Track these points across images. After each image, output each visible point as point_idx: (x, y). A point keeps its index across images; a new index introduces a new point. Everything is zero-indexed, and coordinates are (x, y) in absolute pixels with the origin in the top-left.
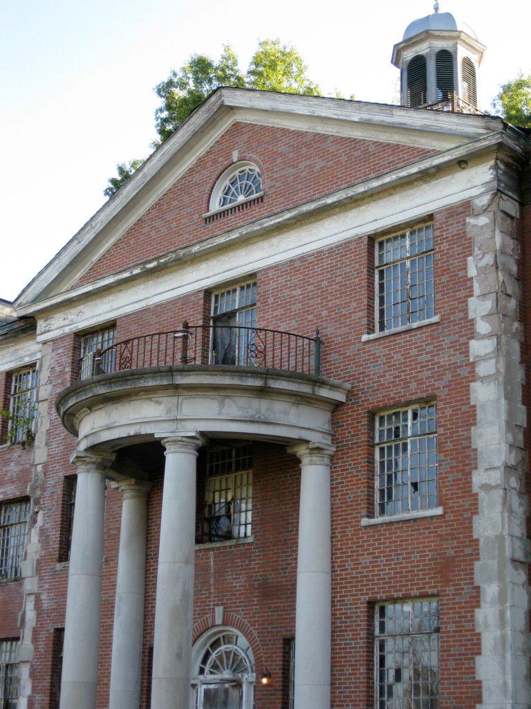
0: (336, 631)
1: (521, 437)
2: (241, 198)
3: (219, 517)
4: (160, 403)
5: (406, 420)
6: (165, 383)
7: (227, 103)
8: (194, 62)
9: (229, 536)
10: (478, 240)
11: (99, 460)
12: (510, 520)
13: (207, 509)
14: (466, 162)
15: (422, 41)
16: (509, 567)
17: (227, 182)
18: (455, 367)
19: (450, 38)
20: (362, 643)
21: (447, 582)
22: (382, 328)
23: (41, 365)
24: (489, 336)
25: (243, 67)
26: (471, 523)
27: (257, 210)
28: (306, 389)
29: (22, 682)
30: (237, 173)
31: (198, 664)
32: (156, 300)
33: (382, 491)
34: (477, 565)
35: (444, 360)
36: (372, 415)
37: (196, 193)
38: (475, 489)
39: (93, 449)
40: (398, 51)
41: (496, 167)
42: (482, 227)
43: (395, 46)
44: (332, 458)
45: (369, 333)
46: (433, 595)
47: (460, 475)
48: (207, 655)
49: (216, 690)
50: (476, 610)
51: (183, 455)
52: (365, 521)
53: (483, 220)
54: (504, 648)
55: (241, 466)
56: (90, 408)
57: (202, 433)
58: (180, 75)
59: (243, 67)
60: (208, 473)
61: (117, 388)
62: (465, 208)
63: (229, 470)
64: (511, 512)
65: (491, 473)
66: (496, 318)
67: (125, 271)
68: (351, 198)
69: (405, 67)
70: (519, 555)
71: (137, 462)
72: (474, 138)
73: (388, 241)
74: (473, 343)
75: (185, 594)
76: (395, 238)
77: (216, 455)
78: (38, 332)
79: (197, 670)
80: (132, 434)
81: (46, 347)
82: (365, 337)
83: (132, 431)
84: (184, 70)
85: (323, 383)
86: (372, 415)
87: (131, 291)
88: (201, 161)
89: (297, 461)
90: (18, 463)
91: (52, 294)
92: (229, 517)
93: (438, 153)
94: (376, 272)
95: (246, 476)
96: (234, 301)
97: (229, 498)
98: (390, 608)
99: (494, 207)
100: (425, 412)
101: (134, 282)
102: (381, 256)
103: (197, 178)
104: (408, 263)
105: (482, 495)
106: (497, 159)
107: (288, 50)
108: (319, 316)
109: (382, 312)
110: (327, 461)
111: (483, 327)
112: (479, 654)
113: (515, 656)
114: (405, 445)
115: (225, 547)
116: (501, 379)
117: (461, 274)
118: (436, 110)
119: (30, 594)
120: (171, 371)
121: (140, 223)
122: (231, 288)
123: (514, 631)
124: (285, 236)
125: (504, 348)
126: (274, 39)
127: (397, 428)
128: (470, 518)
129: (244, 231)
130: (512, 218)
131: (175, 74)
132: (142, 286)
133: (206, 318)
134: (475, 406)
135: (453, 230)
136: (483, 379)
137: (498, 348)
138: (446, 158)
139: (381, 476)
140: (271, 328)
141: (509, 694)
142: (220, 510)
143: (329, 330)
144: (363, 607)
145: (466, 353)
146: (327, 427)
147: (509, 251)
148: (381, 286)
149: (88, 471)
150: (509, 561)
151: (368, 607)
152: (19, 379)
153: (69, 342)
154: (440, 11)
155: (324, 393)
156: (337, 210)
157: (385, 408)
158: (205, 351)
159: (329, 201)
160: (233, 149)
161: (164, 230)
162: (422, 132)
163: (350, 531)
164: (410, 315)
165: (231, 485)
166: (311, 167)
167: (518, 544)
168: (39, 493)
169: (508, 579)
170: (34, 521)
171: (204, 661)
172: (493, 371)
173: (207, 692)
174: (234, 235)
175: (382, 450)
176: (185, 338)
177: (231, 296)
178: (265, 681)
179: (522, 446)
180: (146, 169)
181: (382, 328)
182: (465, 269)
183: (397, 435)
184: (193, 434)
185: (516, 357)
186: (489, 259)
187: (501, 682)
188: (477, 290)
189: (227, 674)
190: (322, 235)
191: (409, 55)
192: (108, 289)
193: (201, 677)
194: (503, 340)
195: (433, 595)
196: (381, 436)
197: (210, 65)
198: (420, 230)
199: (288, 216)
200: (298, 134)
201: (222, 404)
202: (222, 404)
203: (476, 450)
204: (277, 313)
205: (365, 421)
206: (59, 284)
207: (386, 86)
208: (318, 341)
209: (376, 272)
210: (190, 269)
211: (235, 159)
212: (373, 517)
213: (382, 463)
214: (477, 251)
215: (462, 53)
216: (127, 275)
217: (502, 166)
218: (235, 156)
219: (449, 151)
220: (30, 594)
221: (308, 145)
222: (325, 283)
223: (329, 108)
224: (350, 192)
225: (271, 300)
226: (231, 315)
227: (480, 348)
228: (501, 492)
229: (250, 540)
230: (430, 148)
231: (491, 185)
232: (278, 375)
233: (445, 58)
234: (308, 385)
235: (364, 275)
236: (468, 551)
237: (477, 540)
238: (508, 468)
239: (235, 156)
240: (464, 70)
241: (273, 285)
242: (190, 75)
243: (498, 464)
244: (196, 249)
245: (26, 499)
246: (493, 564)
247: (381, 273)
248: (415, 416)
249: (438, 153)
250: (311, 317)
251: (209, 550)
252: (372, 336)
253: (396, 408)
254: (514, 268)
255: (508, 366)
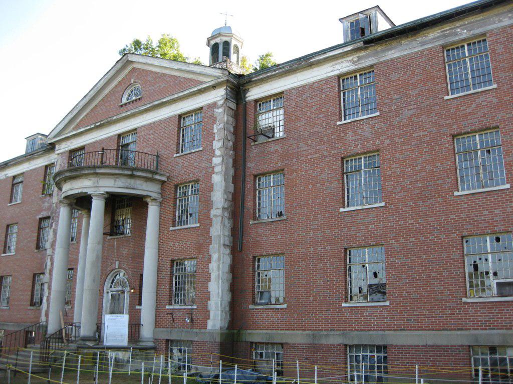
0: (159, 272)
1: (230, 196)
2: (134, 98)
3: (120, 226)
4: (91, 180)
5: (189, 188)
6: (92, 172)
7: (130, 60)
8: (134, 41)
9: (123, 233)
10: (218, 118)
11: (69, 202)
12: (223, 229)
13: (115, 223)
14: (215, 87)
15: (218, 37)
16: (222, 247)
17: (129, 92)
18: (207, 168)
19: (229, 36)
20: (168, 276)
21: (199, 253)
22: (182, 152)
23: (57, 163)
24: (220, 156)
25: (155, 44)
26: (209, 230)
27: (139, 103)
28: (150, 175)
29: (45, 291)
30: (133, 88)
31: (110, 284)
32: (100, 138)
33: (179, 217)
34: (211, 246)
35: (203, 165)
36: (176, 186)
37: (117, 96)
38: (212, 216)
39: (66, 197)
40: (209, 40)
41: (226, 89)
42: (220, 113)
43: (208, 39)
44: (161, 203)
45: (177, 154)
46: (194, 258)
47: (206, 211)
48: (113, 280)
49: (115, 294)
50: (210, 264)
51: (99, 201)
52: (171, 228)
53: (220, 110)
54: (219, 278)
55: (129, 205)
56: (65, 181)
57: (107, 192)
58: (129, 46)
59: (155, 44)
60: (116, 207)
61: (74, 174)
62: (214, 105)
63: (124, 207)
64: (224, 226)
65: (218, 210)
66: (222, 149)
67: (88, 126)
68: (173, 99)
69: (211, 47)
70: (227, 243)
71: (82, 202)
72: (218, 78)
73: (187, 117)
74: (214, 159)
75: (97, 256)
76: (189, 116)
77: (114, 202)
78: (56, 150)
79: (109, 286)
80: (80, 192)
81: (59, 156)
82: (175, 155)
83: (79, 191)
84: (131, 44)
85: (157, 173)
86: (176, 186)
87: (91, 134)
88: (120, 83)
89: (146, 204)
90: (48, 203)
91: (64, 133)
92: (123, 225)
93: (206, 83)
94: (182, 129)
95: (129, 209)
96: (129, 139)
97: (124, 218)
98: (262, 259)
99: (225, 105)
100: (196, 186)
101: (92, 131)
102: (184, 123)
103: (118, 89)
104: (193, 126)
105: (214, 219)
106: (227, 86)
107: (173, 38)
108: (159, 146)
109: (182, 145)
110: (158, 204)
111: (218, 153)
112: (210, 281)
113: (223, 282)
114: (188, 198)
115: (121, 238)
116: (223, 173)
117: (211, 131)
118: (215, 67)
119: (49, 255)
120: (94, 167)
121: (97, 108)
122: (128, 134)
123: (223, 272)
124: (148, 114)
125: (225, 162)
126: (168, 34)
127: (186, 192)
128: (209, 228)
129: (133, 111)
130: (233, 109)
131: (127, 46)
132: (95, 132)
133: (118, 146)
134: (213, 184)
135: (209, 114)
136: (217, 173)
137: (223, 161)
138: (208, 85)
139: (179, 210)
140: (141, 151)
141: (220, 297)
142: (118, 221)
143: (163, 152)
144: (169, 262)
145: (211, 163)
146: (159, 191)
147: (231, 123)
148: (183, 135)
149: (64, 207)
150: (222, 245)
151: (345, 251)
152: (50, 169)
153: (67, 154)
154: (227, 25)
155: (158, 177)
156: (168, 104)
157: (181, 184)
158: (117, 159)
159: (164, 100)
160: (131, 78)
161: (104, 110)
162: (200, 74)
163: (166, 232)
164: (192, 147)
165: (125, 213)
166: (160, 86)
167: (227, 238)
168: (54, 214)
169: (222, 252)
170: (52, 226)
171: (112, 283)
172: (220, 170)
173: (112, 294)
174: (129, 113)
175: (180, 200)
176: (102, 154)
177: (128, 138)
178: (132, 291)
179: (231, 200)
180: (98, 85)
181: (182, 152)
182: (213, 129)
183: (185, 195)
184: (103, 193)
185: (231, 165)
186: (222, 126)
187: (217, 292)
188: (216, 138)
189: (120, 288)
190: (162, 114)
191: (212, 42)
192: (81, 133)
193: (111, 289)
194: (225, 158)
195: (194, 258)
196: (180, 195)
197: (140, 43)
198: (198, 113)
199: (149, 106)
200: (156, 73)
201: (115, 181)
202: (115, 181)
203: (213, 201)
204: (144, 145)
205: (173, 189)
206: (65, 130)
207: (205, 56)
208: (158, 156)
209: (182, 129)
210: (113, 126)
211: (132, 82)
212: (175, 227)
213: (179, 205)
214: (218, 122)
215: (233, 43)
216: (89, 128)
217: (229, 89)
218: (132, 81)
219: (209, 82)
220: (49, 255)
221: (160, 78)
222: (162, 133)
223: (166, 63)
224: (172, 97)
225: (142, 140)
226: (128, 145)
227: (216, 161)
228: (221, 218)
229: (130, 235)
230: (203, 81)
231: (224, 96)
232: (138, 169)
233: (227, 44)
234: (150, 175)
235: (176, 131)
236: (208, 241)
237: (211, 237)
238: (224, 209)
239: (132, 81)
240: (234, 49)
241: (143, 133)
242: (133, 47)
243: (220, 207)
244: (115, 118)
245: (48, 218)
246: (216, 246)
247: (183, 129)
248: (192, 187)
249: (206, 83)
250: (156, 147)
251: (114, 239)
252: (178, 155)
253: (185, 184)
254: (232, 130)
255: (226, 168)
